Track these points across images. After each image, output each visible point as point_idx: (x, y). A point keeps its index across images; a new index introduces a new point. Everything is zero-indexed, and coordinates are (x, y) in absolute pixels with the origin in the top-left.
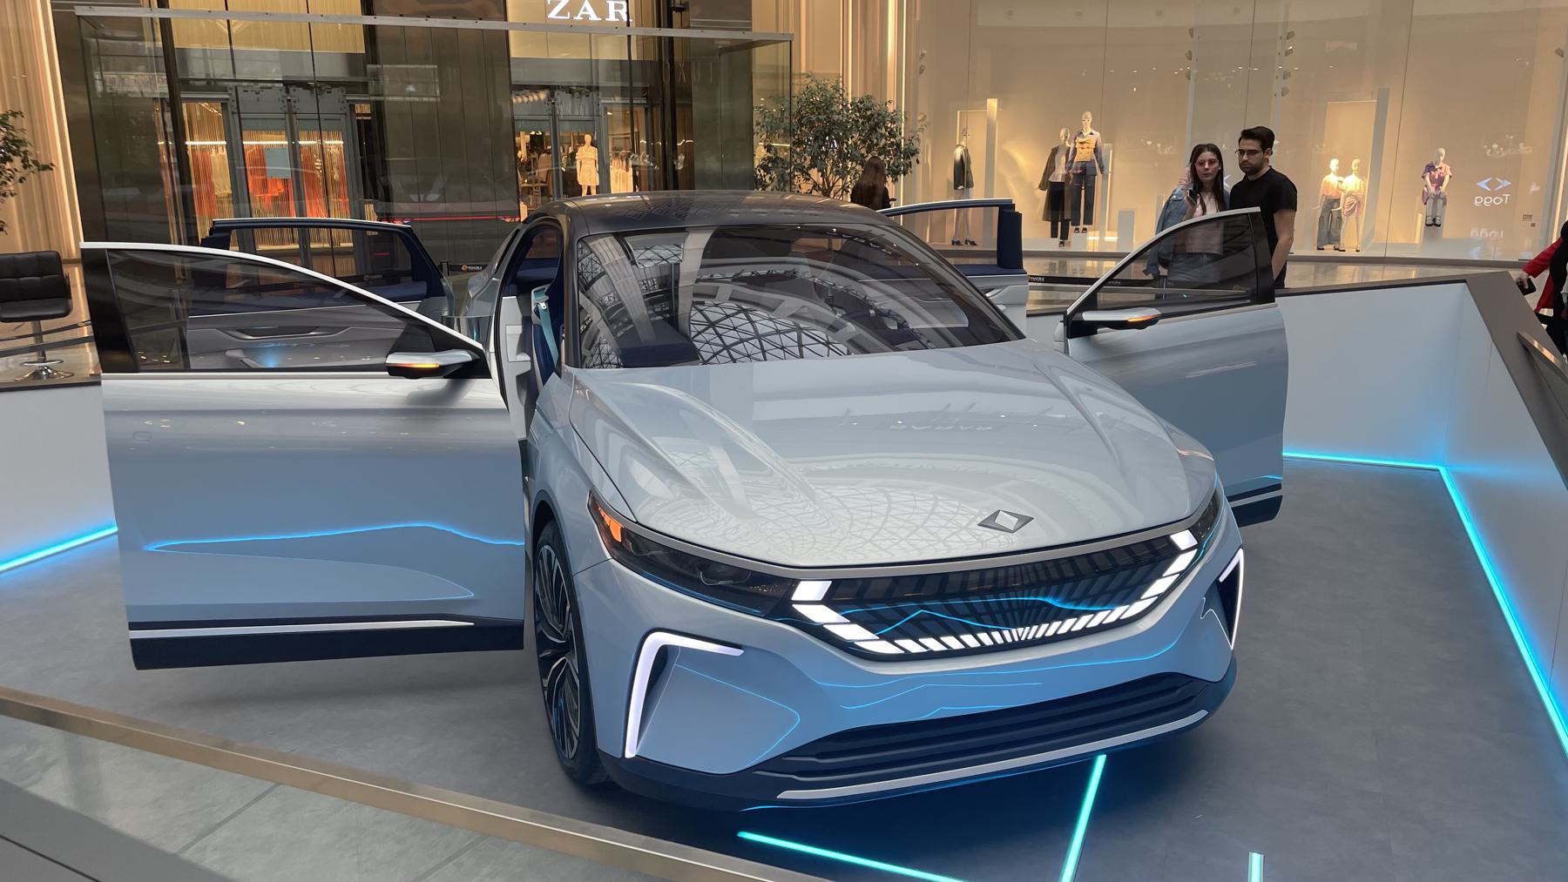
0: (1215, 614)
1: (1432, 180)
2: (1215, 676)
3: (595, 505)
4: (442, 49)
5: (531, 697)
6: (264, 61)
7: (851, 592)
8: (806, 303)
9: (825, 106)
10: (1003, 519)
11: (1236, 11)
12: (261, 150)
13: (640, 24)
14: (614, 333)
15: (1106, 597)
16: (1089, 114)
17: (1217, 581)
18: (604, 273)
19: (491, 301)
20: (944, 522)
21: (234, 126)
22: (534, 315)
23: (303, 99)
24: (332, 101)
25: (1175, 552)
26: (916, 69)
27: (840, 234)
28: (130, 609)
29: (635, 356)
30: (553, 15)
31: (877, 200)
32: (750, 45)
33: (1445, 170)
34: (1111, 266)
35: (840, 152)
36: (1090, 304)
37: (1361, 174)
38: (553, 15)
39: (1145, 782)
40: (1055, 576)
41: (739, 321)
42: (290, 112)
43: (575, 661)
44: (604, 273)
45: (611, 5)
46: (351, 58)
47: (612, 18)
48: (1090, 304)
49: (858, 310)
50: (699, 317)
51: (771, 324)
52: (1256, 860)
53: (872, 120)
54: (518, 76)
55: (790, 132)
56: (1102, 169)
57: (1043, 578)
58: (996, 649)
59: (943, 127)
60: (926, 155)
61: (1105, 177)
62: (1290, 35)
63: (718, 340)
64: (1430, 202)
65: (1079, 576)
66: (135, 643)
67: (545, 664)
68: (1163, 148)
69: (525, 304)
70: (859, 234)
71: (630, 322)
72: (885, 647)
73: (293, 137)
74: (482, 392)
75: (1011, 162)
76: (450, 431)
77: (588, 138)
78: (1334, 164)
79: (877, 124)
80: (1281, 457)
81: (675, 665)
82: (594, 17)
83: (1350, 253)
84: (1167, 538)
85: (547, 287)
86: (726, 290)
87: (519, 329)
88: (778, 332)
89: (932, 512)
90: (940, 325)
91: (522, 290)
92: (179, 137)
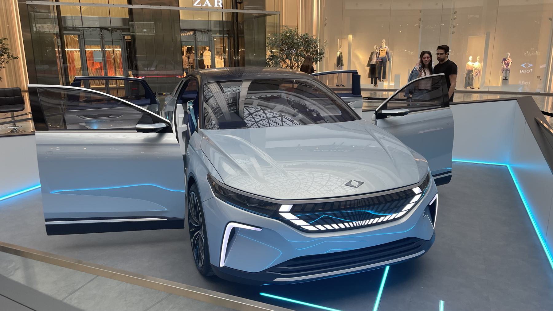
0: (428, 216)
1: (505, 64)
4: (156, 16)
7: (301, 209)
9: (291, 37)
10: (353, 183)
14: (217, 117)
15: (396, 209)
16: (384, 40)
18: (213, 96)
19: (173, 105)
20: (332, 184)
22: (188, 111)
23: (107, 34)
24: (117, 35)
25: (414, 194)
26: (323, 24)
27: (296, 82)
29: (224, 125)
30: (195, 5)
32: (265, 15)
33: (510, 60)
36: (384, 107)
37: (480, 62)
38: (195, 5)
41: (261, 112)
42: (102, 39)
44: (213, 96)
46: (124, 20)
47: (216, 6)
48: (384, 107)
49: (303, 109)
51: (272, 114)
53: (308, 42)
54: (183, 26)
55: (279, 46)
57: (364, 204)
58: (351, 229)
59: (333, 45)
60: (327, 54)
61: (390, 63)
62: (455, 13)
63: (264, 115)
64: (505, 72)
69: (185, 107)
70: (304, 83)
71: (222, 113)
72: (311, 228)
73: (103, 48)
74: (170, 138)
75: (357, 58)
76: (159, 152)
77: (207, 48)
78: (471, 58)
79: (310, 44)
81: (238, 234)
82: (210, 5)
83: (476, 89)
84: (411, 190)
85: (193, 101)
86: (256, 102)
87: (183, 116)
88: (274, 117)
90: (331, 115)
91: (184, 102)
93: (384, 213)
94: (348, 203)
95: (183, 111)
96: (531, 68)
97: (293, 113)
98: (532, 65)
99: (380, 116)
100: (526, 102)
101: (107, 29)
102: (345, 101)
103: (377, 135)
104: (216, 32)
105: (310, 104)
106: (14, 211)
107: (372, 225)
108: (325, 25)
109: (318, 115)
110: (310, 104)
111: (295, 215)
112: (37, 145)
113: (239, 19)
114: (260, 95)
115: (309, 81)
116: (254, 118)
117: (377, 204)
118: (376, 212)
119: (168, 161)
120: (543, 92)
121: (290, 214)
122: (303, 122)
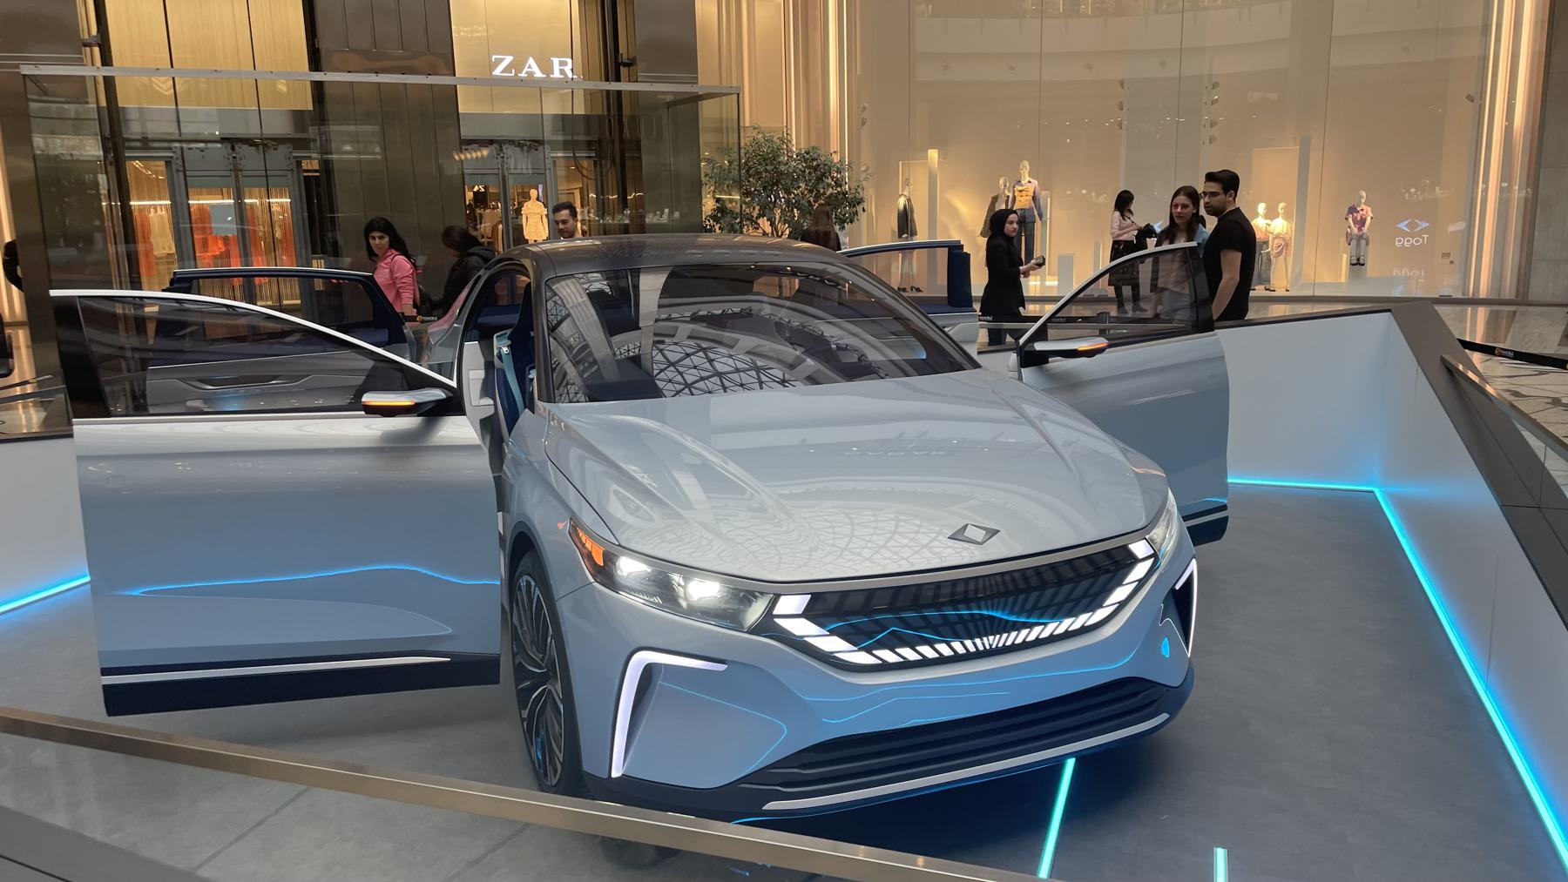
0: (1171, 622)
1: (1355, 220)
2: (1175, 681)
3: (576, 526)
4: (387, 109)
5: (510, 731)
6: (203, 120)
7: (829, 606)
8: (761, 342)
9: (772, 157)
10: (971, 532)
11: (1163, 64)
12: (201, 208)
13: (588, 76)
14: (581, 374)
15: (1070, 605)
16: (1026, 163)
17: (1173, 589)
18: (569, 315)
19: (452, 346)
20: (905, 542)
21: (180, 182)
22: (496, 360)
23: (247, 154)
24: (279, 157)
25: (1133, 560)
26: (858, 121)
27: (794, 273)
28: (101, 654)
29: (598, 392)
30: (497, 72)
31: (833, 243)
32: (697, 98)
33: (1367, 212)
34: (1050, 309)
35: (788, 202)
36: (1041, 335)
37: (1287, 217)
38: (497, 72)
39: (1114, 783)
40: (1022, 585)
41: (699, 359)
42: (236, 169)
43: (559, 686)
44: (569, 315)
45: (556, 61)
46: (298, 117)
47: (557, 74)
48: (1041, 335)
49: (817, 347)
50: (659, 357)
51: (730, 361)
52: (1220, 854)
53: (817, 169)
54: (466, 132)
55: (738, 184)
56: (1041, 216)
57: (1011, 587)
58: (968, 657)
59: (886, 177)
60: (871, 205)
61: (1044, 224)
62: (1215, 85)
63: (679, 378)
64: (1354, 243)
65: (1043, 585)
66: (107, 689)
67: (523, 696)
68: (1098, 196)
69: (487, 349)
70: (814, 273)
71: (595, 362)
72: (863, 658)
73: (239, 197)
74: (459, 430)
75: (954, 212)
76: (426, 467)
77: (533, 193)
78: (1261, 208)
79: (823, 174)
80: (1226, 485)
81: (659, 682)
82: (538, 74)
83: (1281, 292)
84: (1125, 548)
85: (509, 332)
86: (685, 329)
87: (481, 374)
88: (738, 370)
89: (895, 532)
90: (895, 357)
91: (485, 336)
92: (124, 196)
93: (1041, 617)
94: (960, 588)
95: (482, 361)
96: (1424, 231)
97: (790, 361)
98: (1425, 225)
99: (1030, 359)
100: (1416, 317)
101: (249, 142)
102: (940, 323)
103: (1031, 411)
104: (554, 145)
105: (835, 332)
106: (36, 630)
107: (1025, 646)
108: (863, 123)
109: (862, 356)
110: (835, 332)
111: (821, 625)
112: (80, 458)
113: (626, 111)
114: (695, 308)
115: (830, 269)
116: (711, 361)
117: (1035, 589)
118: (1012, 613)
119: (450, 495)
120: (1459, 296)
121: (803, 621)
122: (812, 380)
